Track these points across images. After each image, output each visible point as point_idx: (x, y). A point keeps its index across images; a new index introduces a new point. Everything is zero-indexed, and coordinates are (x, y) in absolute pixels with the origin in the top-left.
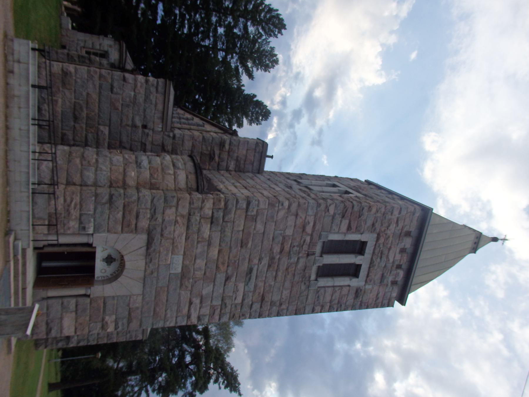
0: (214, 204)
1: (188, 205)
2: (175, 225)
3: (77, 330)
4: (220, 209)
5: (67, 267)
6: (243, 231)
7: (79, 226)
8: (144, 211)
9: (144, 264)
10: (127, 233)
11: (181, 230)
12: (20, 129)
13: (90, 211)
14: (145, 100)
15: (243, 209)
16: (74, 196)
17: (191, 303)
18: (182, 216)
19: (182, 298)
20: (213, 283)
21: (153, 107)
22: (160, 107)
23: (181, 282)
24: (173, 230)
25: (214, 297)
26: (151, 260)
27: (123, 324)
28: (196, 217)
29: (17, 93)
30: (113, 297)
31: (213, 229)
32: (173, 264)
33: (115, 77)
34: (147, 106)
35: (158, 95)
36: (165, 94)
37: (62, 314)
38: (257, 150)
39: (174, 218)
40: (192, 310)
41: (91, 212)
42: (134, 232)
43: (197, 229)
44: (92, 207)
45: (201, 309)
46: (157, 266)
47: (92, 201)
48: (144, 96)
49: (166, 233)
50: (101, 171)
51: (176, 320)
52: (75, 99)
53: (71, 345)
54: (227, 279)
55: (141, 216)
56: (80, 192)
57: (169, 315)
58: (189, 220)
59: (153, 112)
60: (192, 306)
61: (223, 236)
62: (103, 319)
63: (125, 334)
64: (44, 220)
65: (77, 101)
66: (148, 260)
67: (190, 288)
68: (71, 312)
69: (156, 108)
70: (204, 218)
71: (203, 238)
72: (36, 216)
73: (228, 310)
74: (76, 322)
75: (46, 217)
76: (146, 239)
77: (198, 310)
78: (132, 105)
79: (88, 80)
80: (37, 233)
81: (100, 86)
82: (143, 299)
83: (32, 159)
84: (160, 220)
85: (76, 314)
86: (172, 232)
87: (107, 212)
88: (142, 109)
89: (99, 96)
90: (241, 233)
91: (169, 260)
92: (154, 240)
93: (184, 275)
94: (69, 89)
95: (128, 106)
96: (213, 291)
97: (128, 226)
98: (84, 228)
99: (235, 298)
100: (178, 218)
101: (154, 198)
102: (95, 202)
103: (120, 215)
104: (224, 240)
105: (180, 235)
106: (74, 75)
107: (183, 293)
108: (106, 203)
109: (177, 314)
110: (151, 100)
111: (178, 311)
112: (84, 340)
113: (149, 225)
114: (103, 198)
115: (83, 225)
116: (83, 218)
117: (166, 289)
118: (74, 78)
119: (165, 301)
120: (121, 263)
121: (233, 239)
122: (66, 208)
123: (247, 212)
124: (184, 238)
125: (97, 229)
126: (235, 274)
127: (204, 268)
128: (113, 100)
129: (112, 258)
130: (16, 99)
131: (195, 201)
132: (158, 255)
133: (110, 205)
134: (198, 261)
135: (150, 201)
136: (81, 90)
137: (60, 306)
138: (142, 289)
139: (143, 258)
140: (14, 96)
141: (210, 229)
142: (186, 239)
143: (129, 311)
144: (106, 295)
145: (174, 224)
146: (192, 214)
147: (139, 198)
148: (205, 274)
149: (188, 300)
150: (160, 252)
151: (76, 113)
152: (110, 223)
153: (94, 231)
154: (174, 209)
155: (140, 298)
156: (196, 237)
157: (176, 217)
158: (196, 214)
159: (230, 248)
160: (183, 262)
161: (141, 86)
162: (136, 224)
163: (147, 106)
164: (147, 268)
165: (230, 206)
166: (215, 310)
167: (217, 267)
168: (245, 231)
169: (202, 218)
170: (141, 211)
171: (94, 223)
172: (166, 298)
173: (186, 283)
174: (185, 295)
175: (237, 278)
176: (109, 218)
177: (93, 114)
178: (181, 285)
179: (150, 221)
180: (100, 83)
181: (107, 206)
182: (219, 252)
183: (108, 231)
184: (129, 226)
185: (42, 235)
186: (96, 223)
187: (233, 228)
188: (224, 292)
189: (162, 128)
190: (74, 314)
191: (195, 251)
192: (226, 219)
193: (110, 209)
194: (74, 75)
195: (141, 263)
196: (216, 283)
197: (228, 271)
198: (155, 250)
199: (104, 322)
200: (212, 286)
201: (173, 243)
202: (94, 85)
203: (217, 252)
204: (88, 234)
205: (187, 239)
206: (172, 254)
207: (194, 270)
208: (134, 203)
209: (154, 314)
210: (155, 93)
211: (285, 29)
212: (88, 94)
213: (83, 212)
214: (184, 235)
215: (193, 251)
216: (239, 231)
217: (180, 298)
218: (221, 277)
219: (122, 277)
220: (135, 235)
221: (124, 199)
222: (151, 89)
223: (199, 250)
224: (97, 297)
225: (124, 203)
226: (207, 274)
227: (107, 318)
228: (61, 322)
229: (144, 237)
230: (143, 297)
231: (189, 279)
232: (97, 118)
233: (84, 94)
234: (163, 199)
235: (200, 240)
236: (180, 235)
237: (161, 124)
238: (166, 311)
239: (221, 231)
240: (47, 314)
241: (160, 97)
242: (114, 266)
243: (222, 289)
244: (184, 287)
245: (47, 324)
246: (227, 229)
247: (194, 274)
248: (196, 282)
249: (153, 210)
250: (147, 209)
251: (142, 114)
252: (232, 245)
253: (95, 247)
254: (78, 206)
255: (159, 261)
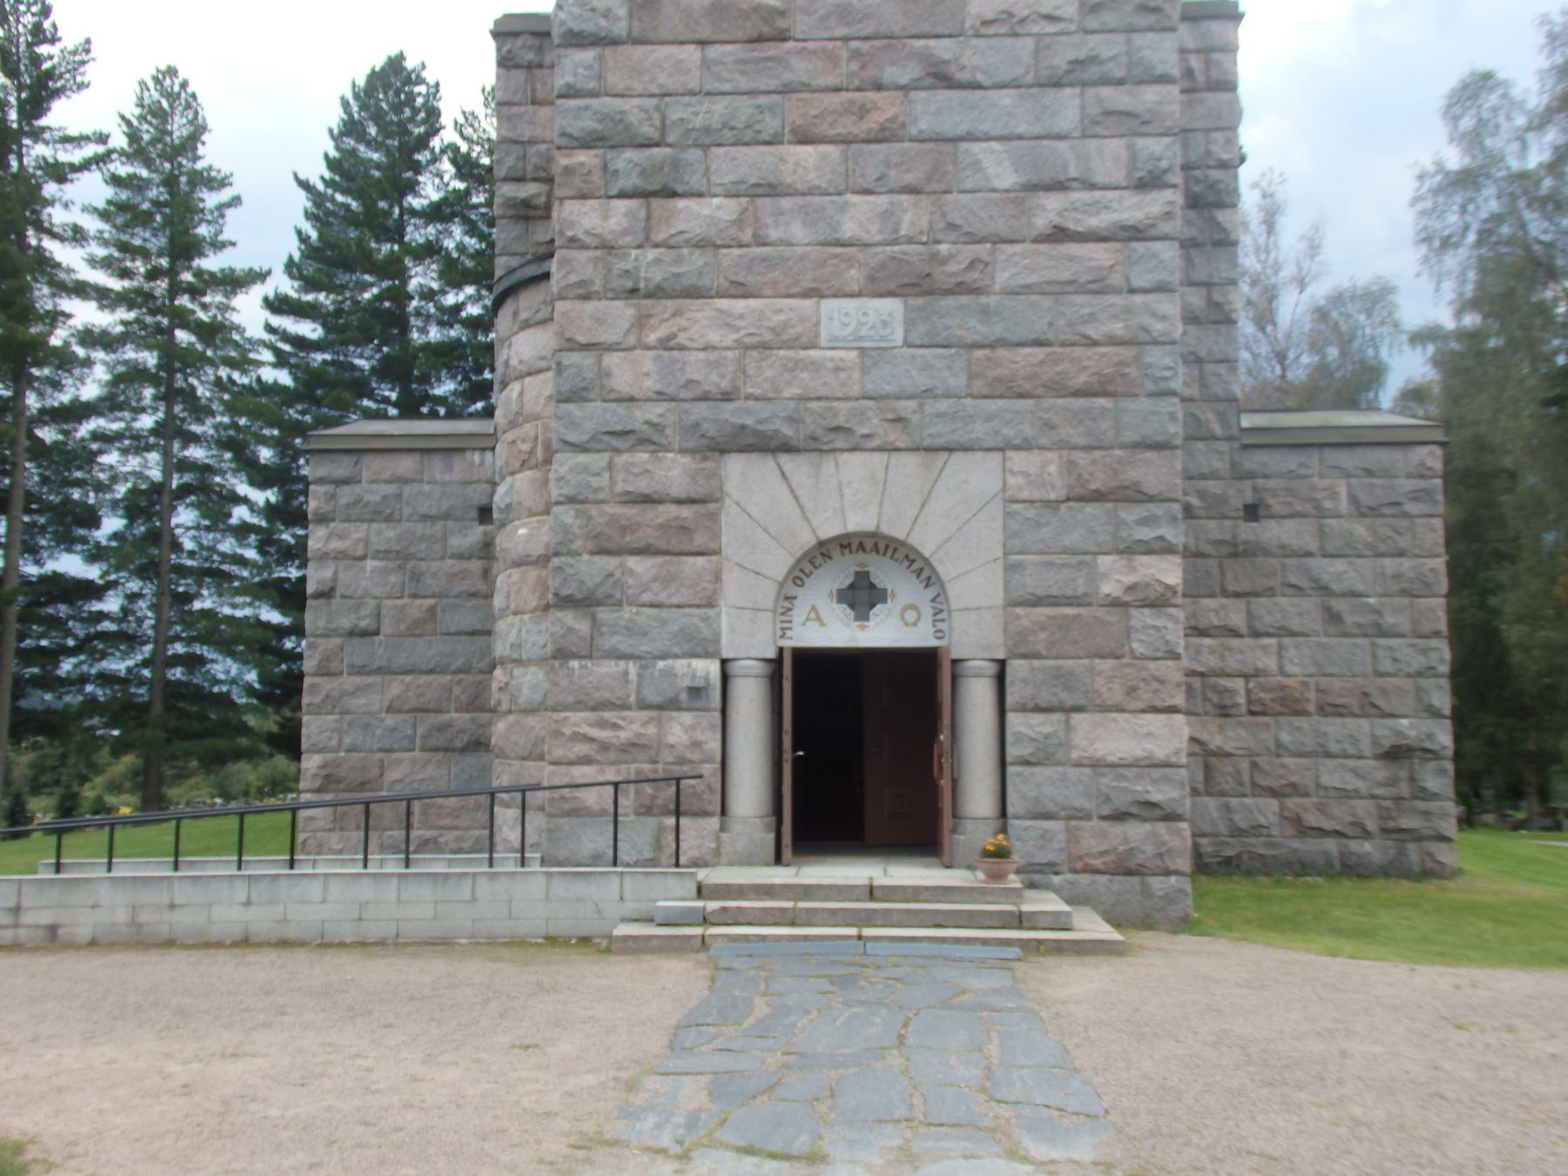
0: (583, 197)
1: (591, 306)
2: (682, 348)
3: (1159, 704)
4: (605, 167)
5: (860, 751)
6: (702, 43)
7: (689, 709)
8: (620, 476)
9: (857, 458)
10: (716, 536)
11: (703, 323)
12: (248, 903)
13: (626, 673)
14: (388, 519)
15: (601, 58)
16: (568, 731)
17: (1059, 234)
18: (641, 322)
19: (1033, 279)
20: (964, 145)
21: (408, 490)
22: (406, 465)
23: (950, 292)
24: (701, 355)
25: (1037, 129)
26: (837, 429)
27: (1146, 521)
28: (649, 265)
29: (122, 916)
30: (1011, 569)
31: (695, 181)
32: (861, 338)
33: (321, 624)
34: (407, 511)
35: (365, 475)
36: (359, 451)
37: (1078, 765)
38: (530, 56)
39: (651, 353)
40: (1097, 222)
41: (633, 668)
42: (712, 506)
43: (697, 252)
44: (609, 668)
45: (1099, 179)
46: (870, 403)
47: (582, 667)
48: (374, 526)
49: (715, 381)
50: (520, 646)
51: (1145, 291)
52: (413, 750)
53: (1444, 738)
54: (941, 78)
55: (643, 486)
56: (554, 709)
57: (1118, 328)
58: (658, 293)
59: (426, 487)
60: (1071, 226)
61: (728, 134)
62: (1116, 603)
63: (1405, 523)
64: (661, 829)
65: (418, 742)
66: (840, 443)
67: (982, 250)
68: (1068, 727)
69: (413, 481)
70: (647, 231)
71: (739, 222)
72: (648, 855)
73: (1108, 47)
74: (1120, 709)
75: (651, 822)
76: (742, 457)
77: (1097, 194)
78: (410, 565)
79: (345, 712)
80: (717, 852)
81: (361, 671)
82: (1025, 446)
83: (365, 866)
84: (654, 412)
85: (1078, 709)
86: (713, 356)
87: (627, 612)
88: (420, 529)
89: (394, 673)
90: (714, 52)
91: (842, 354)
92: (743, 427)
93: (915, 284)
94: (382, 767)
95: (416, 577)
96: (1001, 139)
97: (689, 529)
98: (696, 692)
99: (1050, 18)
100: (652, 338)
101: (566, 442)
102: (590, 657)
103: (640, 566)
104: (748, 127)
105: (727, 322)
106: (330, 756)
107: (1003, 277)
108: (594, 619)
109: (1117, 291)
110: (385, 497)
111: (1098, 286)
112: (1419, 690)
113: (682, 451)
114: (570, 629)
115: (683, 697)
116: (654, 698)
117: (980, 353)
118: (342, 754)
119: (1040, 353)
120: (876, 549)
121: (743, 83)
122: (612, 755)
123: (614, 42)
124: (739, 305)
125: (704, 647)
126: (919, 44)
127: (883, 201)
128: (403, 627)
129: (852, 586)
130: (144, 917)
131: (573, 279)
132: (813, 405)
133: (599, 603)
134: (849, 230)
135: (582, 458)
136: (378, 732)
137: (1038, 770)
138: (979, 455)
139: (828, 463)
140: (134, 924)
141: (700, 195)
142: (744, 296)
143: (1081, 499)
144: (998, 598)
145: (676, 354)
146: (630, 284)
147: (571, 500)
148: (913, 190)
149: (1042, 247)
150: (802, 399)
151: (458, 744)
152: (674, 601)
153: (707, 655)
154: (612, 360)
155: (1017, 459)
156: (736, 251)
157: (648, 348)
158: (629, 266)
159: (786, 90)
160: (852, 296)
161: (341, 537)
162: (680, 502)
163: (407, 511)
164: (875, 443)
165: (589, 123)
166: (1108, 113)
167: (882, 136)
168: (705, 33)
169: (647, 238)
170: (620, 487)
171: (676, 657)
172: (1027, 350)
173: (952, 267)
174: (1014, 266)
175: (940, 31)
176: (652, 605)
177: (457, 691)
178: (961, 289)
179: (667, 449)
180: (350, 674)
181: (603, 614)
182: (804, 139)
183: (711, 604)
184: (685, 530)
185: (724, 836)
186: (676, 650)
187: (693, 93)
188: (1014, 84)
189: (483, 449)
190: (1076, 718)
191: (799, 250)
192: (649, 131)
193: (619, 604)
194: (330, 756)
195: (855, 467)
196: (961, 130)
197: (903, 81)
198: (792, 420)
199: (1127, 598)
200: (976, 147)
201: (764, 346)
202: (357, 691)
203: (809, 149)
204: (725, 678)
205: (741, 290)
206: (813, 345)
207: (895, 242)
208: (590, 518)
209: (1105, 394)
210: (357, 489)
211: (401, 57)
212: (390, 710)
213: (632, 699)
214: (724, 304)
215: (802, 258)
216: (706, 64)
217: (1028, 289)
218: (933, 112)
219: (914, 540)
220: (727, 501)
221: (576, 554)
222: (343, 501)
223: (798, 232)
224: (1005, 630)
225: (593, 553)
226: (909, 178)
227: (1108, 588)
228: (1113, 766)
229: (735, 467)
230: (1017, 448)
231: (934, 258)
232: (469, 678)
233: (390, 721)
234: (571, 407)
235: (747, 236)
236: (727, 322)
237: (468, 455)
238: (1095, 343)
239: (705, 148)
240: (1069, 818)
241: (372, 466)
242: (885, 574)
243: (993, 94)
244: (975, 275)
245: (1119, 817)
246: (698, 122)
247: (910, 241)
248: (952, 226)
249: (615, 442)
250: (610, 467)
251: (439, 526)
252: (773, 84)
253: (781, 650)
254: (607, 715)
255: (847, 399)
